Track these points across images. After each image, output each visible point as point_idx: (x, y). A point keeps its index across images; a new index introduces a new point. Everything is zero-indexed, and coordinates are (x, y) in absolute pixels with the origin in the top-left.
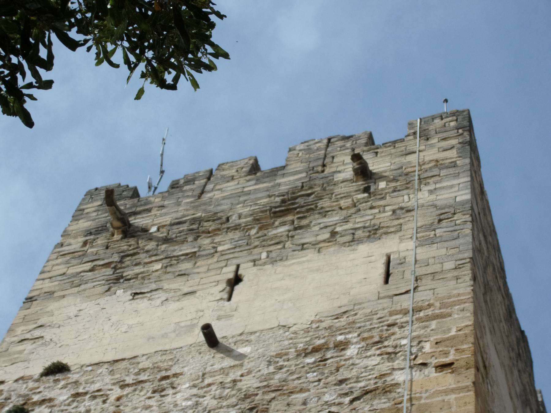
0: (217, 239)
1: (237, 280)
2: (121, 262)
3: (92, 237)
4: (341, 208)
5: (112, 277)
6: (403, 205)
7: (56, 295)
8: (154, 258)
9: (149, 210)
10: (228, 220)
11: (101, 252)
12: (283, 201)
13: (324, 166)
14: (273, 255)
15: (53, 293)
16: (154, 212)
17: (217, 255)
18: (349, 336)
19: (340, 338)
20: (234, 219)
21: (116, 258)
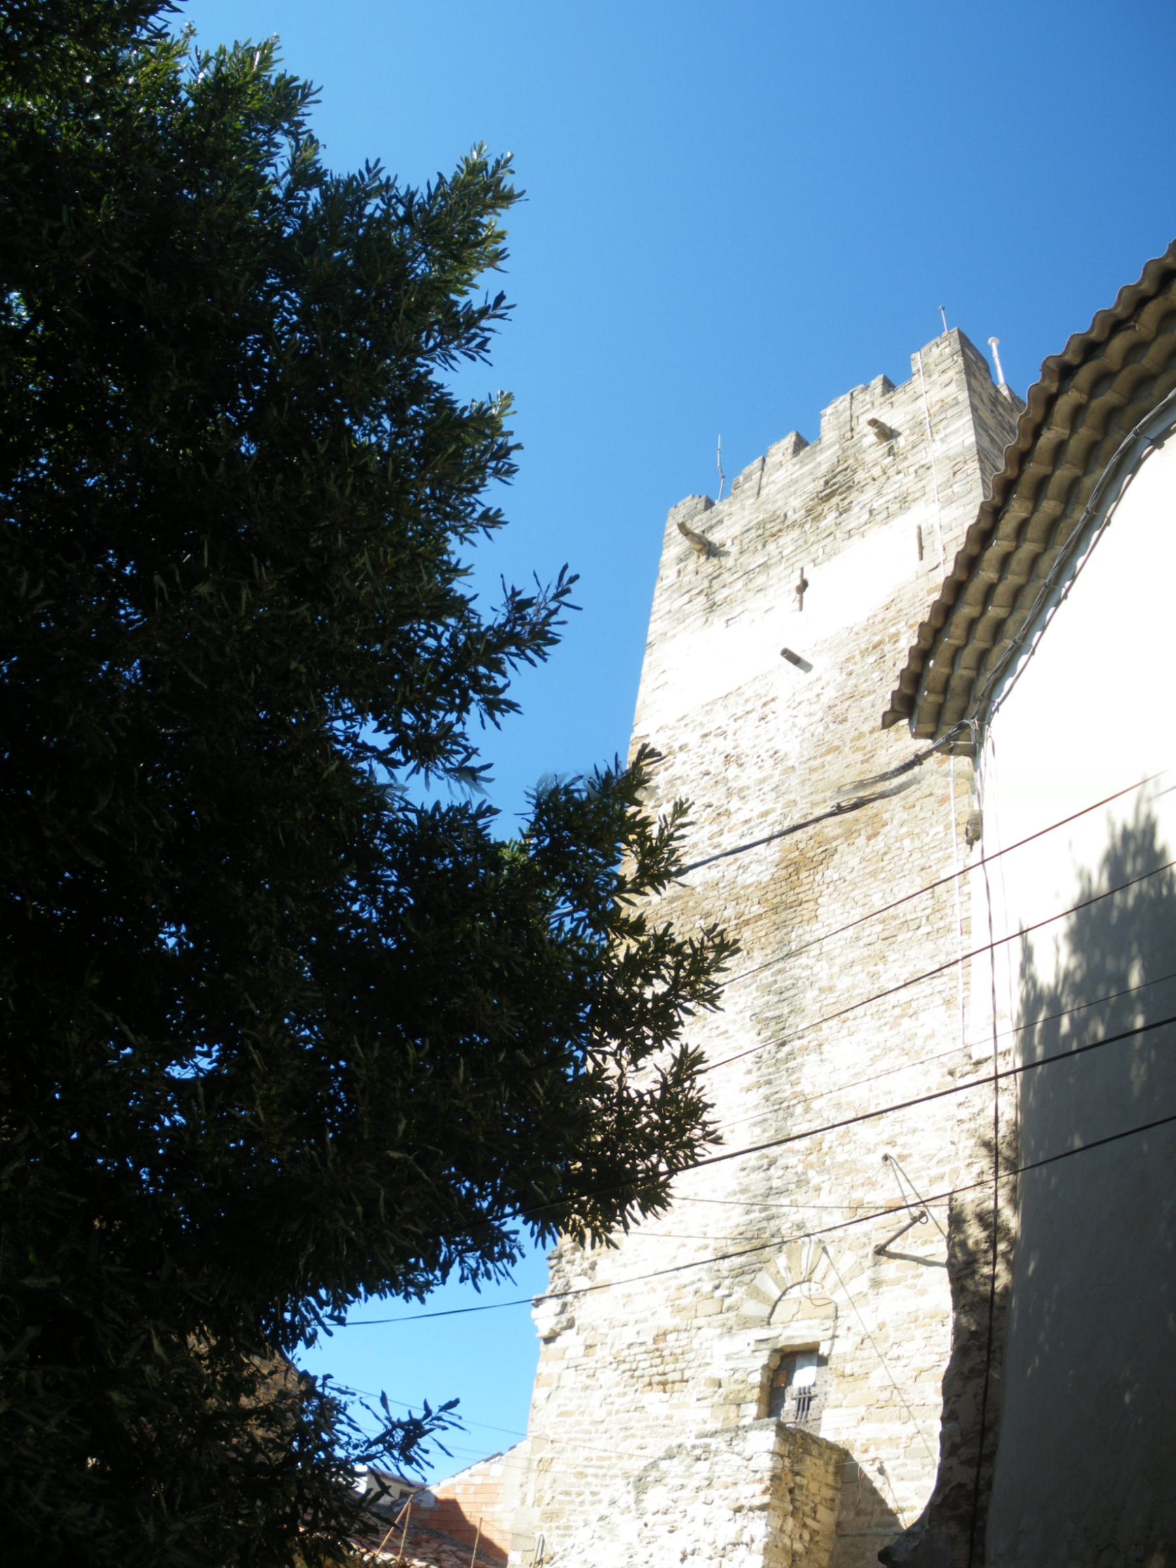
0: (781, 541)
1: (804, 585)
2: (710, 587)
3: (683, 564)
4: (874, 479)
5: (707, 605)
6: (923, 462)
7: (669, 635)
8: (735, 576)
9: (721, 522)
10: (786, 516)
11: (693, 579)
12: (827, 483)
13: (852, 430)
14: (828, 549)
15: (665, 634)
16: (726, 523)
17: (784, 560)
18: (899, 626)
19: (893, 630)
20: (792, 517)
21: (706, 584)
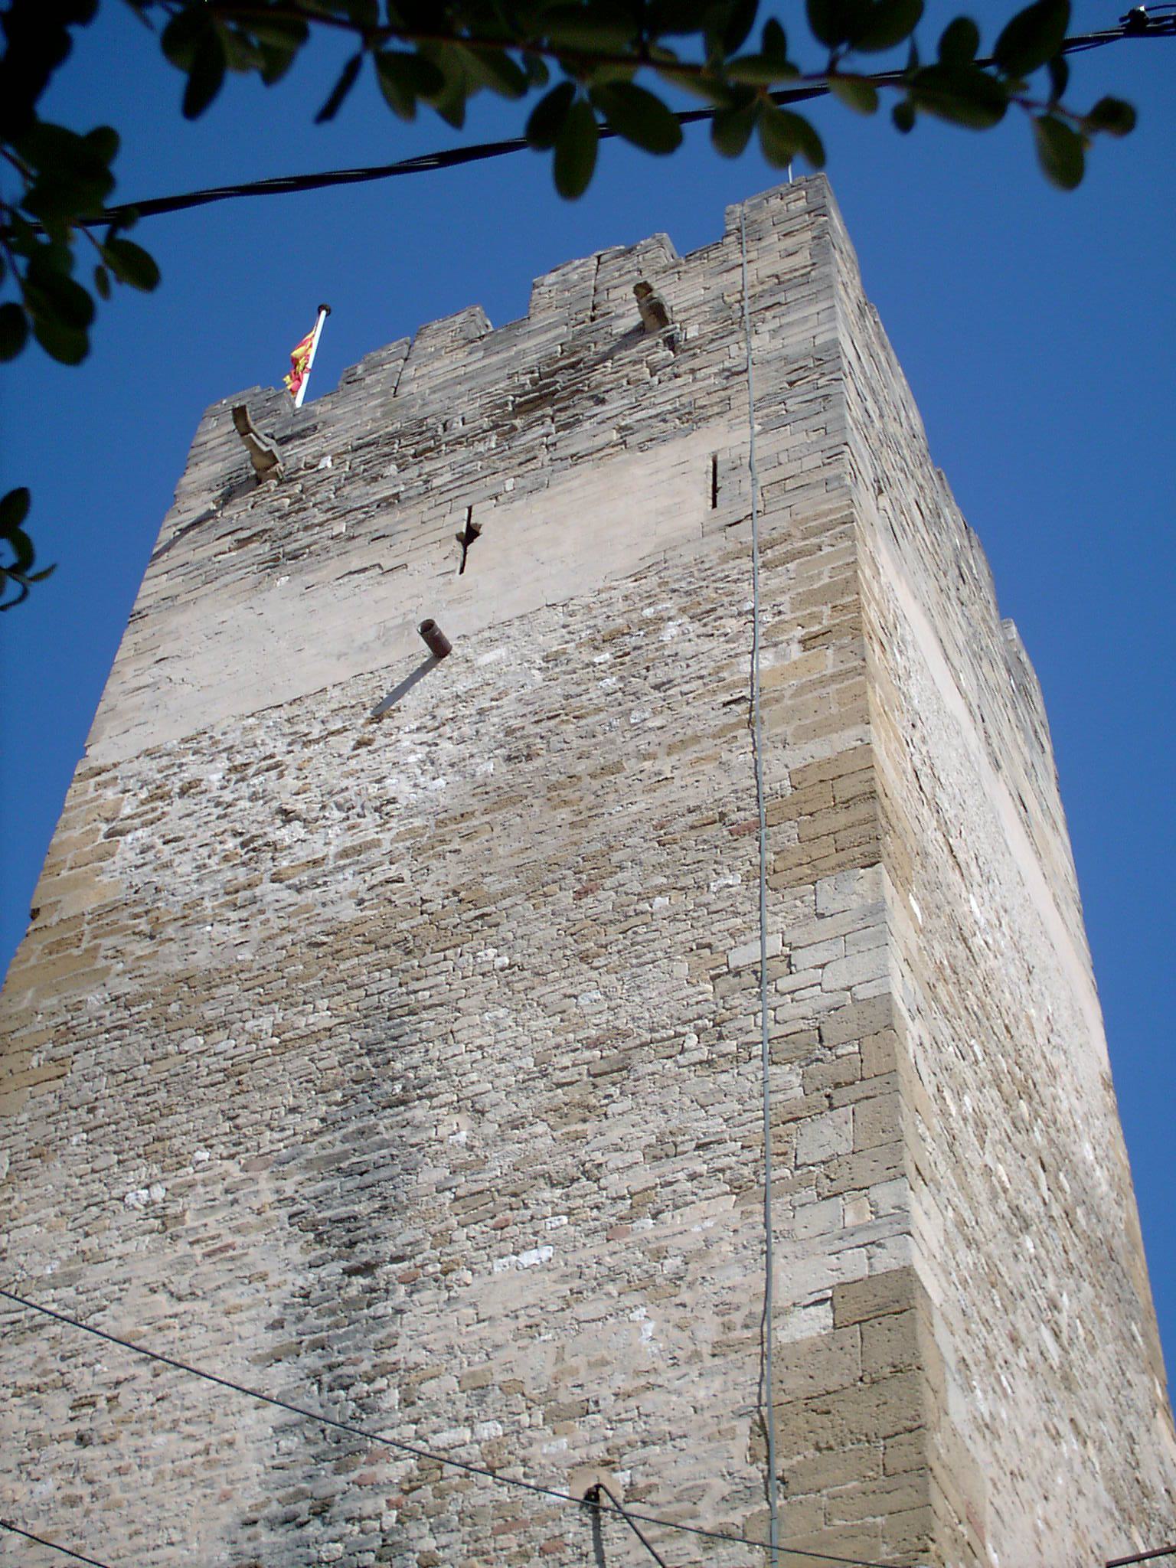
1: (471, 534)
